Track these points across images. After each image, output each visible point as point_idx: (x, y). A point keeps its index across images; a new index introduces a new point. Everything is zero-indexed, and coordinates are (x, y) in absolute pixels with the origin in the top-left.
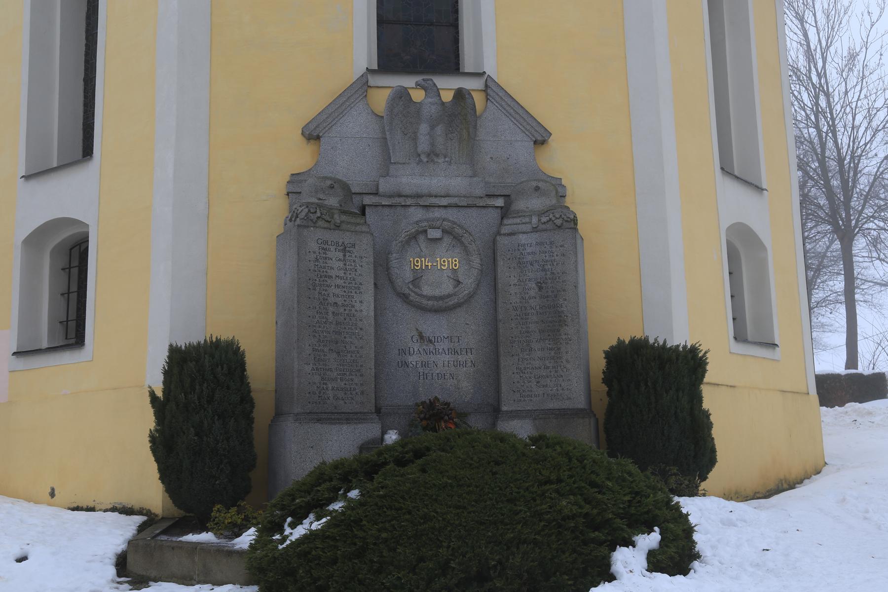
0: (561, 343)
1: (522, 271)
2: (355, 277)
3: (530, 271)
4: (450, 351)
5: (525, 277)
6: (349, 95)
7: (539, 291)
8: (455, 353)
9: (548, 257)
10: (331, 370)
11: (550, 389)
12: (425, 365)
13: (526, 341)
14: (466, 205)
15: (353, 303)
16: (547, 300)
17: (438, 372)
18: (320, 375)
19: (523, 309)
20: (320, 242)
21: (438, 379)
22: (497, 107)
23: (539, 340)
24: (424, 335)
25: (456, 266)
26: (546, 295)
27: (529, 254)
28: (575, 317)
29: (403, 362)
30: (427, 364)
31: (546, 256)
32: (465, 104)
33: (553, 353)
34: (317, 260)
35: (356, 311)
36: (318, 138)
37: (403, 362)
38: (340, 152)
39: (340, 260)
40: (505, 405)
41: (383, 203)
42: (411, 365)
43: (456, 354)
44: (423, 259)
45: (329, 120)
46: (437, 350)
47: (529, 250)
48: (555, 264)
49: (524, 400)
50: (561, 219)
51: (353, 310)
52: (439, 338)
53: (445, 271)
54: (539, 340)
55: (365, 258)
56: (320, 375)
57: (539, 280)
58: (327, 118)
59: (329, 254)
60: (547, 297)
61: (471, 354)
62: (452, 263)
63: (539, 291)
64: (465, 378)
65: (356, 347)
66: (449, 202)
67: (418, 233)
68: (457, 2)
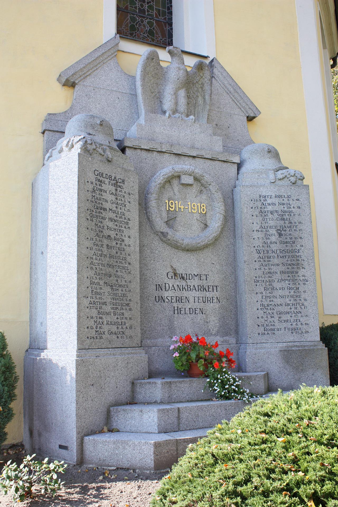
0: (299, 284)
1: (264, 219)
2: (125, 212)
3: (271, 219)
4: (200, 287)
5: (267, 225)
6: (104, 51)
7: (279, 237)
8: (203, 289)
9: (286, 208)
10: (105, 303)
11: (291, 323)
12: (179, 300)
13: (268, 281)
14: (211, 158)
15: (123, 238)
16: (287, 246)
17: (190, 307)
18: (97, 309)
19: (265, 252)
20: (96, 173)
21: (190, 314)
22: (220, 84)
23: (280, 280)
24: (178, 272)
25: (203, 211)
26: (285, 241)
27: (269, 204)
28: (311, 261)
29: (160, 297)
30: (180, 299)
31: (284, 208)
32: (203, 75)
33: (292, 291)
34: (94, 191)
35: (125, 245)
36: (73, 85)
37: (160, 297)
38: (94, 100)
39: (112, 194)
40: (250, 337)
41: (142, 147)
42: (167, 300)
43: (204, 290)
44: (177, 202)
45: (85, 70)
46: (189, 286)
47: (269, 201)
48: (292, 214)
49: (268, 334)
50: (295, 177)
51: (123, 244)
52: (190, 275)
53: (195, 215)
54: (280, 280)
55: (132, 195)
56: (97, 309)
57: (279, 228)
58: (84, 67)
59: (104, 187)
60: (286, 243)
61: (217, 291)
62: (201, 207)
63: (279, 237)
64: (212, 313)
65: (125, 281)
66: (198, 153)
67: (173, 177)
68: (171, 2)
